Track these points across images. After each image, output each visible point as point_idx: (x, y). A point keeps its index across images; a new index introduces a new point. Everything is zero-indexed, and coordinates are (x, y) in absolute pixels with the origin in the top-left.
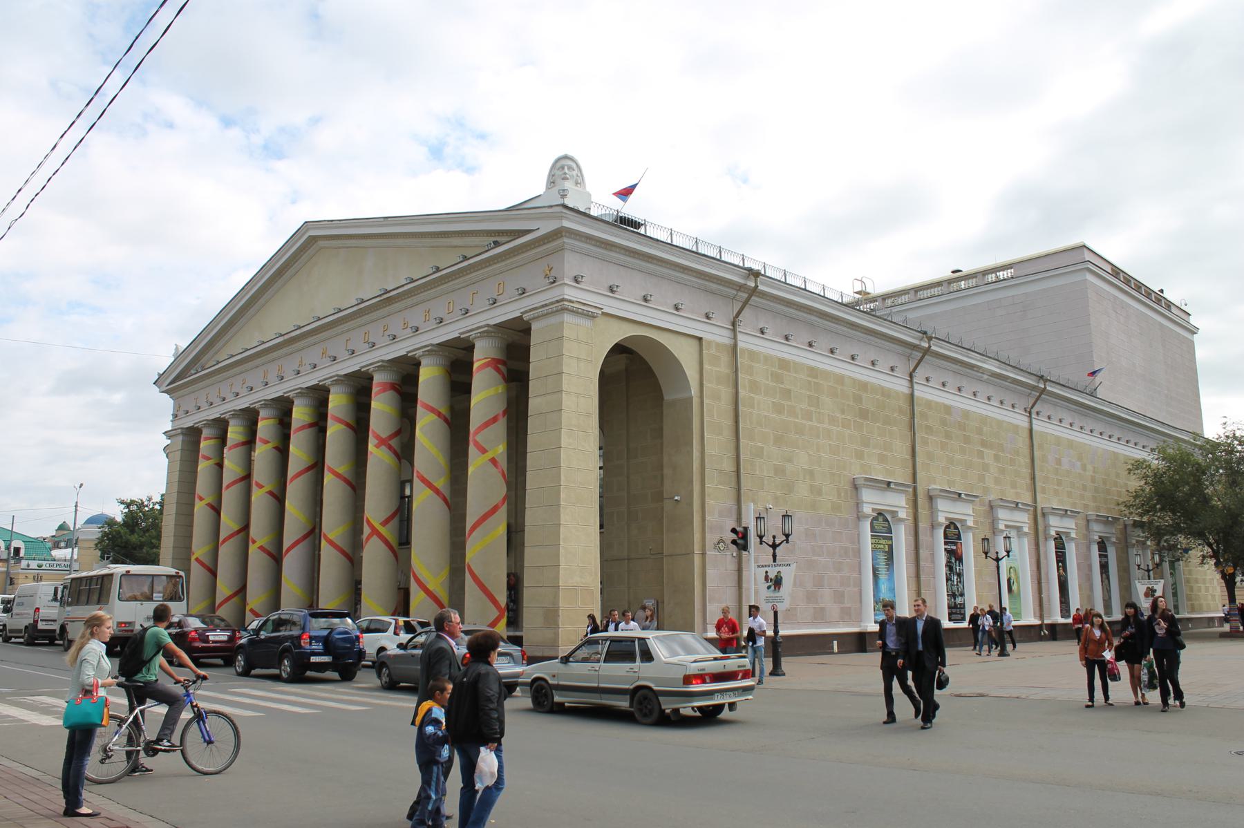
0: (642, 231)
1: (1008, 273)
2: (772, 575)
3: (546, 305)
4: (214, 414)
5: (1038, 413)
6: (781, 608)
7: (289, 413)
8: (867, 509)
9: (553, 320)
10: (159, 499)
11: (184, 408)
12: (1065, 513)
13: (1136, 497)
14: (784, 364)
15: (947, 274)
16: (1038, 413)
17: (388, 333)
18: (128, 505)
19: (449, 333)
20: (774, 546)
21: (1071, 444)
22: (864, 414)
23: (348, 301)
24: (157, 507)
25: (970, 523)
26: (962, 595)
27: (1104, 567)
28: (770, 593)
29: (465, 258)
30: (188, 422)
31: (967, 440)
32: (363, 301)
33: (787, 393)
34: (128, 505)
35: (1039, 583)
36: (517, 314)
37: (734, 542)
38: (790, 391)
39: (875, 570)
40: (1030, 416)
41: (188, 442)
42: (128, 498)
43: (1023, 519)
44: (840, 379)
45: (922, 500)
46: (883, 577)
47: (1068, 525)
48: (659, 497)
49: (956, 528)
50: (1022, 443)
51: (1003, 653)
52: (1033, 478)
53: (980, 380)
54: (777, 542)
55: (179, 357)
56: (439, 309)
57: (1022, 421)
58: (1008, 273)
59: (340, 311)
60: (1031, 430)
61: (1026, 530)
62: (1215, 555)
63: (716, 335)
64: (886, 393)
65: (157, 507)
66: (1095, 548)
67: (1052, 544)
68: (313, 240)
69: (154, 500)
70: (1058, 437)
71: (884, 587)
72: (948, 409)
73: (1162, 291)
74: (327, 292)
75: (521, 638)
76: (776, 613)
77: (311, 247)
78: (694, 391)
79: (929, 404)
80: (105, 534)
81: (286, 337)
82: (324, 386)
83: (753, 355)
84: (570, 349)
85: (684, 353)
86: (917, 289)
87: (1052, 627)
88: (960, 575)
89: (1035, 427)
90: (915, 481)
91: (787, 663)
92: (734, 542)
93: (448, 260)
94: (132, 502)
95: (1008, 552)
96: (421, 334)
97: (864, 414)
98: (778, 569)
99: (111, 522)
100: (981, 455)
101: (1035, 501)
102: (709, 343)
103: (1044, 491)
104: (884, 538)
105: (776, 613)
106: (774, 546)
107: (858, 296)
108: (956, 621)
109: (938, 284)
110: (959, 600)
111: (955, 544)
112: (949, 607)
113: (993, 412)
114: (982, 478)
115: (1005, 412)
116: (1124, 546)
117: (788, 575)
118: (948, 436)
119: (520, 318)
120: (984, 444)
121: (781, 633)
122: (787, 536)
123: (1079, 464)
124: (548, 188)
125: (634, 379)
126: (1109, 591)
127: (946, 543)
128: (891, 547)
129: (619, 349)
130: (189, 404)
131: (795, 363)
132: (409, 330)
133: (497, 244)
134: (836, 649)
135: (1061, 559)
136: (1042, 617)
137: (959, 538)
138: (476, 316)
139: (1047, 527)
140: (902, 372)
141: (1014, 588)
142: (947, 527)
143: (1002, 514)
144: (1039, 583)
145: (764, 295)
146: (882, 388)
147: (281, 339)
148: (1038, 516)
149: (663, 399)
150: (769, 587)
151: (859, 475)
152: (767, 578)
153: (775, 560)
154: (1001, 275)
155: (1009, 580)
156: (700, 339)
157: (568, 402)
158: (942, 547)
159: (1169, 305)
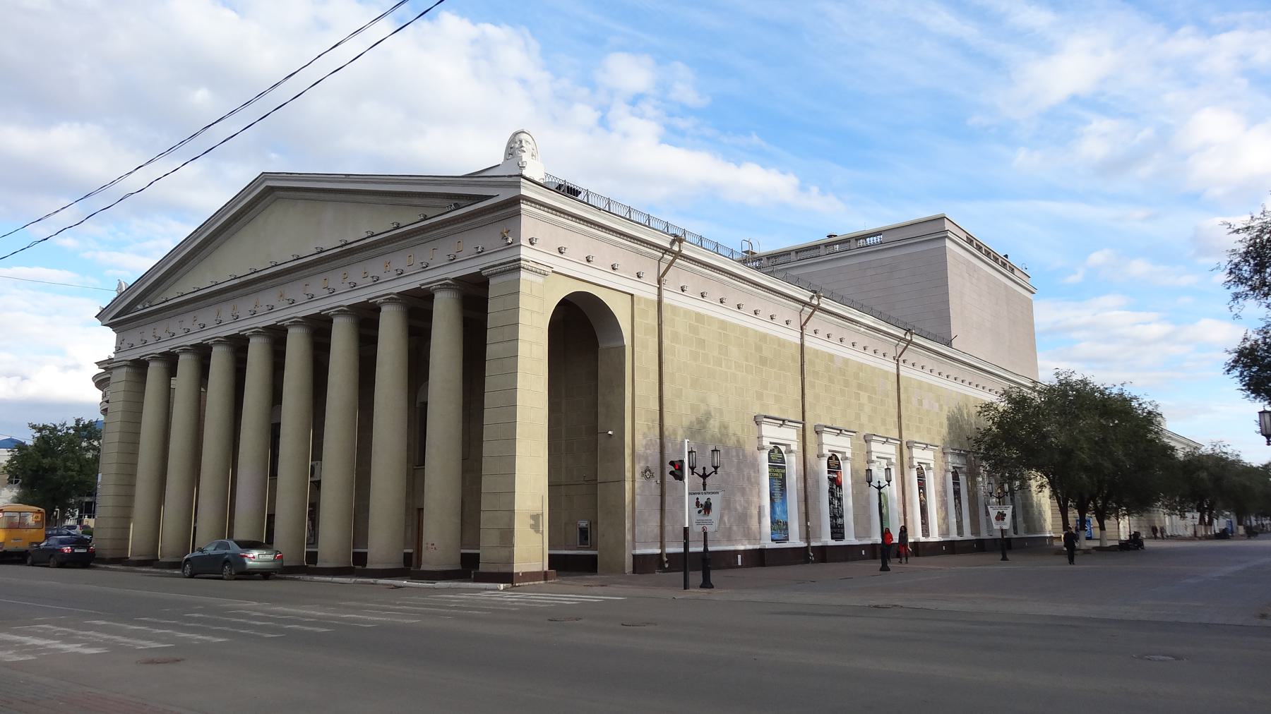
0: (580, 197)
2: (702, 501)
6: (710, 529)
8: (766, 443)
9: (509, 277)
10: (73, 424)
13: (984, 435)
14: (700, 318)
15: (820, 237)
17: (348, 280)
18: (40, 430)
20: (704, 476)
21: (930, 388)
23: (308, 250)
24: (72, 431)
25: (848, 455)
26: (842, 517)
27: (957, 493)
28: (701, 517)
31: (846, 383)
33: (702, 343)
34: (40, 430)
39: (772, 495)
42: (40, 422)
43: (891, 450)
44: (745, 331)
45: (810, 435)
46: (778, 501)
49: (780, 452)
51: (885, 568)
52: (900, 417)
53: (858, 332)
55: (121, 296)
57: (890, 367)
60: (802, 345)
62: (1051, 483)
64: (782, 344)
65: (72, 431)
66: (950, 476)
67: (915, 473)
68: (271, 190)
69: (68, 425)
70: (921, 382)
71: (778, 510)
72: (831, 357)
74: (284, 239)
77: (267, 196)
79: (816, 352)
80: (14, 458)
81: (243, 279)
83: (674, 308)
84: (525, 303)
86: (798, 251)
88: (840, 500)
89: (806, 344)
91: (715, 576)
92: (672, 473)
93: (409, 218)
94: (45, 427)
96: (384, 281)
97: (763, 361)
99: (21, 446)
100: (858, 396)
101: (901, 436)
102: (640, 298)
105: (705, 534)
106: (704, 476)
109: (817, 247)
110: (839, 521)
114: (858, 417)
116: (972, 475)
117: (716, 501)
118: (831, 380)
119: (479, 273)
120: (860, 387)
121: (691, 550)
122: (716, 468)
123: (937, 405)
124: (506, 159)
125: (581, 328)
126: (960, 514)
128: (784, 475)
130: (134, 336)
131: (710, 318)
132: (369, 279)
133: (458, 207)
135: (922, 486)
136: (808, 539)
137: (839, 468)
138: (438, 266)
139: (911, 458)
140: (795, 324)
142: (830, 458)
143: (875, 447)
146: (779, 339)
148: (905, 447)
151: (757, 411)
152: (697, 504)
154: (870, 240)
157: (523, 349)
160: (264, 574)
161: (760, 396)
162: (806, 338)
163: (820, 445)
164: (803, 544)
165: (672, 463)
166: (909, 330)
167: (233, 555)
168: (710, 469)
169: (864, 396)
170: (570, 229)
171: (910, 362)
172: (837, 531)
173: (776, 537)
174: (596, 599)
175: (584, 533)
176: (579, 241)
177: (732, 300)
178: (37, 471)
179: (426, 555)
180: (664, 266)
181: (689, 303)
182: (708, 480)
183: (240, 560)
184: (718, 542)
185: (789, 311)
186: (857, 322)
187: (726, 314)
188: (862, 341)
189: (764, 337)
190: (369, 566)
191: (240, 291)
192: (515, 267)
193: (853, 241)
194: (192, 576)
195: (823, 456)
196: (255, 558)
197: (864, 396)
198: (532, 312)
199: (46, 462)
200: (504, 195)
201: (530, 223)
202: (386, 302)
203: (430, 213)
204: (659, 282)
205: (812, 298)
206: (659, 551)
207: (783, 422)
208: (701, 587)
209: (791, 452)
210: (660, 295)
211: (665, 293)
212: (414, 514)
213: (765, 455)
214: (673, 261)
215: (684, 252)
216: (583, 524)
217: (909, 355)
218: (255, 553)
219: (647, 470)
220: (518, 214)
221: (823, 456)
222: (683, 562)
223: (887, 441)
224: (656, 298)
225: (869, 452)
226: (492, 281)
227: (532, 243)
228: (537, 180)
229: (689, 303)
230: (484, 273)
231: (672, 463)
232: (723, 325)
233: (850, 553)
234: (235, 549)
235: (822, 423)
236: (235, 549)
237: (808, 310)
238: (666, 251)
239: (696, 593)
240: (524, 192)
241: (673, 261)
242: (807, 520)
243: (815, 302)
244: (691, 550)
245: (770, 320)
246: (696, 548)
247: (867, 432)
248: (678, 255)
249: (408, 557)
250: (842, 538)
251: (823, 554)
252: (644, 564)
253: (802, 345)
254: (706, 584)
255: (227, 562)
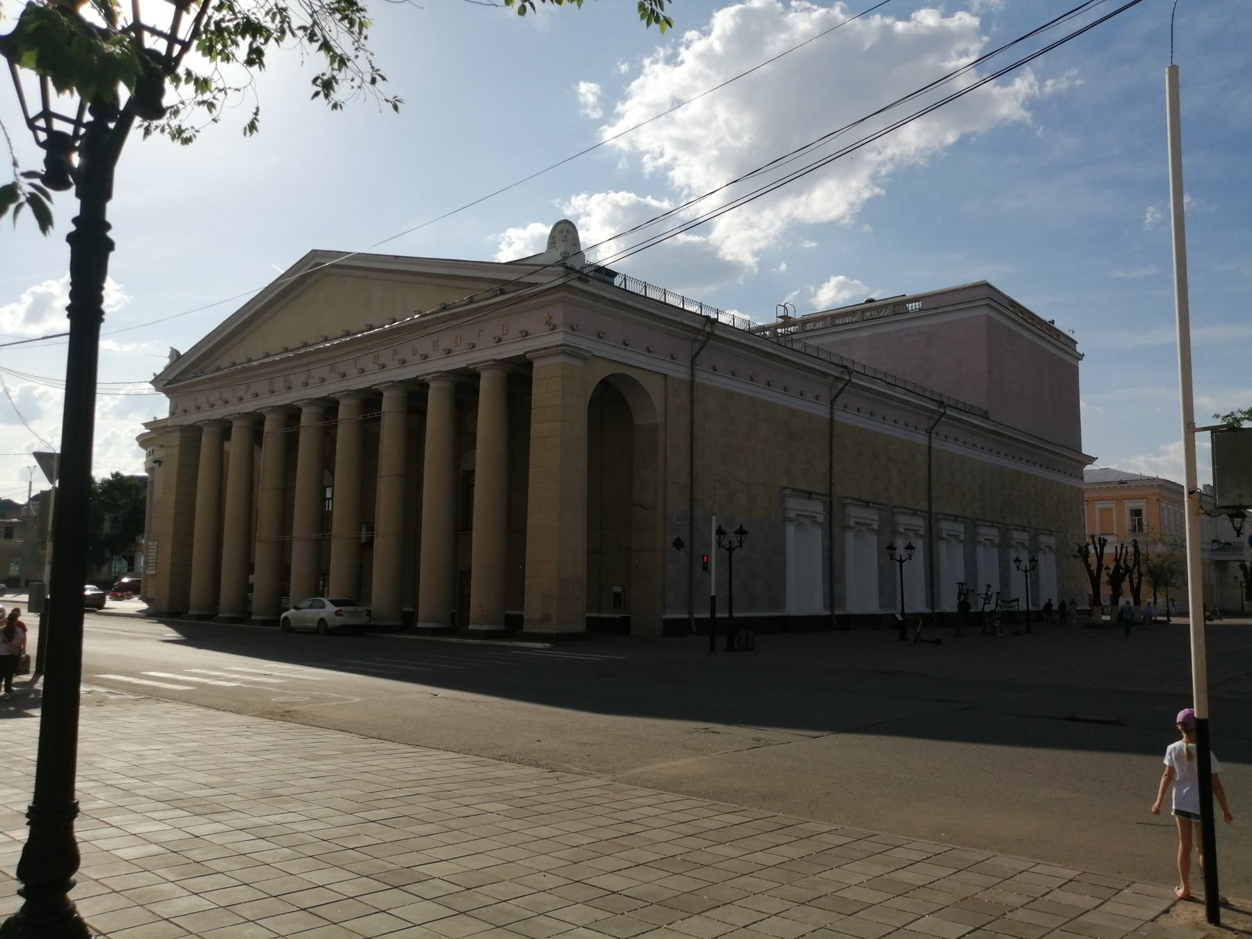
1: (917, 305)
4: (219, 413)
12: (956, 519)
14: (731, 395)
19: (459, 362)
30: (190, 420)
43: (919, 522)
52: (930, 489)
56: (446, 341)
58: (917, 305)
60: (930, 447)
63: (679, 371)
73: (1053, 322)
85: (653, 387)
89: (933, 445)
96: (434, 361)
101: (930, 507)
107: (780, 320)
109: (853, 313)
113: (900, 433)
119: (523, 356)
121: (718, 615)
129: (604, 383)
132: (418, 357)
133: (503, 292)
145: (717, 336)
159: (1059, 334)
181: (722, 382)
187: (740, 387)
190: (526, 629)
202: (433, 379)
206: (686, 616)
207: (809, 495)
212: (460, 579)
216: (617, 589)
219: (678, 540)
222: (711, 628)
223: (915, 513)
224: (828, 416)
226: (536, 364)
227: (649, 351)
229: (722, 382)
233: (849, 623)
241: (706, 342)
244: (718, 615)
246: (722, 614)
249: (509, 619)
252: (674, 629)
253: (930, 447)
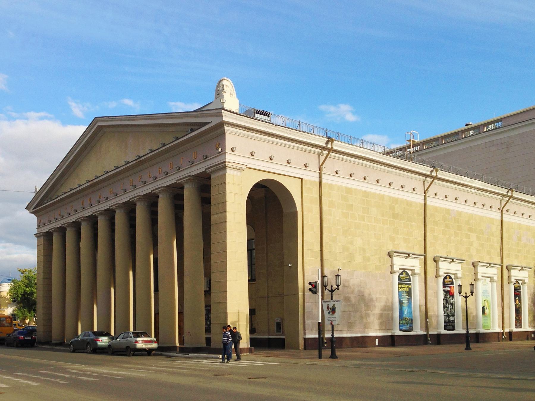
2: (331, 306)
3: (217, 165)
5: (507, 211)
6: (335, 323)
7: (96, 223)
8: (396, 268)
9: (221, 173)
11: (42, 221)
14: (349, 191)
16: (507, 211)
17: (142, 180)
22: (395, 216)
26: (453, 315)
29: (177, 139)
30: (46, 229)
32: (128, 163)
34: (24, 272)
35: (503, 308)
36: (203, 170)
37: (310, 289)
38: (352, 205)
40: (502, 213)
41: (46, 239)
43: (494, 272)
44: (382, 197)
45: (430, 264)
47: (523, 275)
48: (282, 264)
50: (496, 229)
51: (468, 348)
52: (502, 249)
54: (333, 289)
58: (492, 126)
59: (117, 168)
60: (425, 204)
61: (495, 278)
64: (409, 204)
72: (448, 211)
74: (111, 157)
75: (211, 338)
76: (333, 326)
78: (299, 208)
79: (436, 209)
81: (91, 182)
82: (112, 209)
83: (331, 186)
84: (230, 188)
87: (510, 334)
88: (452, 304)
90: (425, 253)
92: (310, 289)
95: (472, 293)
97: (395, 216)
98: (333, 303)
100: (468, 236)
102: (306, 181)
103: (509, 256)
104: (407, 284)
105: (333, 326)
108: (449, 330)
109: (456, 134)
110: (451, 318)
111: (450, 287)
112: (445, 322)
113: (478, 211)
114: (468, 250)
115: (486, 211)
118: (447, 226)
120: (470, 230)
122: (338, 286)
127: (444, 287)
128: (410, 289)
130: (45, 220)
132: (152, 179)
133: (192, 130)
134: (377, 344)
136: (427, 329)
139: (509, 277)
140: (420, 190)
141: (487, 311)
144: (503, 308)
147: (89, 184)
148: (505, 269)
149: (282, 212)
150: (329, 313)
151: (390, 248)
153: (332, 299)
154: (492, 126)
155: (483, 308)
156: (302, 179)
158: (441, 288)
160: (148, 352)
161: (392, 239)
162: (428, 199)
163: (437, 270)
164: (423, 333)
165: (310, 284)
166: (511, 189)
167: (91, 339)
168: (335, 287)
169: (473, 237)
170: (259, 140)
171: (511, 211)
172: (450, 324)
173: (404, 328)
174: (258, 364)
175: (279, 325)
176: (264, 147)
177: (372, 178)
178: (24, 295)
179: (53, 335)
180: (322, 158)
182: (334, 293)
183: (94, 342)
184: (341, 331)
185: (417, 182)
186: (469, 186)
188: (472, 199)
189: (396, 201)
191: (91, 189)
192: (222, 167)
193: (481, 127)
194: (74, 351)
195: (439, 276)
196: (103, 341)
197: (473, 237)
198: (235, 194)
199: (28, 290)
200: (214, 121)
201: (232, 137)
203: (179, 136)
204: (320, 169)
205: (432, 171)
208: (331, 357)
209: (415, 274)
210: (320, 178)
211: (323, 176)
213: (396, 276)
214: (328, 154)
215: (335, 148)
216: (278, 320)
217: (512, 206)
218: (102, 338)
220: (224, 133)
221: (439, 276)
225: (476, 274)
227: (233, 151)
228: (234, 110)
230: (208, 171)
231: (310, 284)
232: (366, 194)
234: (92, 337)
235: (440, 255)
236: (92, 337)
237: (430, 180)
238: (323, 148)
239: (326, 362)
240: (225, 119)
241: (328, 154)
242: (510, 316)
243: (434, 174)
245: (404, 188)
247: (475, 259)
248: (331, 150)
250: (454, 329)
251: (438, 339)
253: (425, 204)
254: (333, 356)
255: (88, 343)
